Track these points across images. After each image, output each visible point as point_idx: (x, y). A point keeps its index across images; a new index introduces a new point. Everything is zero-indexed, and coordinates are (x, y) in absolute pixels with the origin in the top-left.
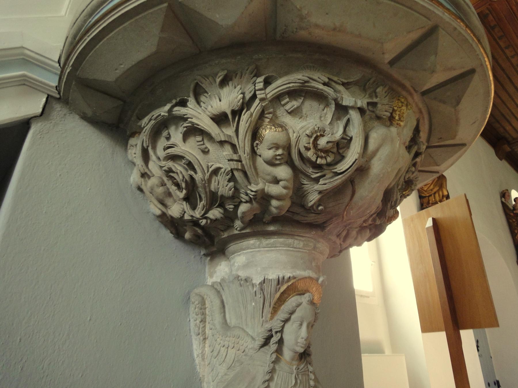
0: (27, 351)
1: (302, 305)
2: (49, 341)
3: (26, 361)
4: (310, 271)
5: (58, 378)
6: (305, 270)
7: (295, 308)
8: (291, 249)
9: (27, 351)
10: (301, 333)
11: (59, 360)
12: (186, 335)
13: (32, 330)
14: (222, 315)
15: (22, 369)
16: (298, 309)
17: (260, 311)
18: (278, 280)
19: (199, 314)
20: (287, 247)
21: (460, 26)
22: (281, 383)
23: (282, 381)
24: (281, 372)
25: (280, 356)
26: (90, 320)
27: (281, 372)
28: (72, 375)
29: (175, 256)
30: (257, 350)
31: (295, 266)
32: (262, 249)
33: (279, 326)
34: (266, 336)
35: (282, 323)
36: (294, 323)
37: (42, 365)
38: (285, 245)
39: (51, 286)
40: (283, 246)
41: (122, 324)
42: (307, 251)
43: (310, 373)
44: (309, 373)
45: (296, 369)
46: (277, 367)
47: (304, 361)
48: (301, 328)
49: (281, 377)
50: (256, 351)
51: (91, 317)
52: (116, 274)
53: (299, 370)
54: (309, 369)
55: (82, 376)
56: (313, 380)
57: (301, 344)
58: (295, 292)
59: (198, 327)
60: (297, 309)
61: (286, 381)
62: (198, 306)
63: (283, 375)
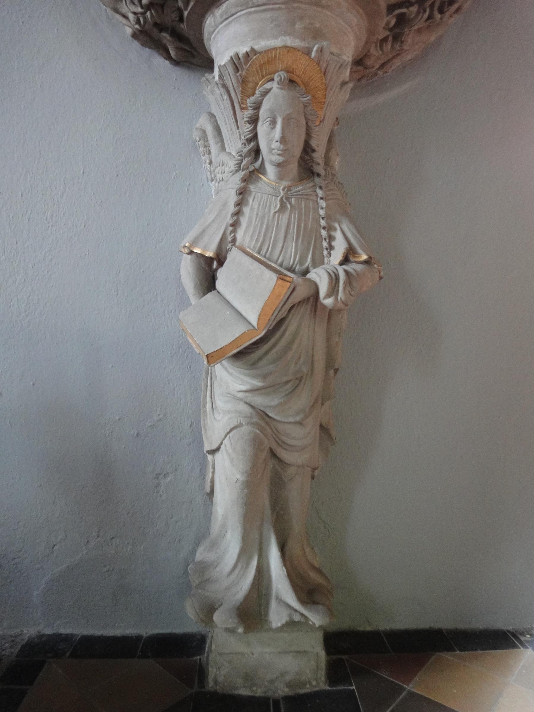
0: (29, 204)
1: (272, 91)
2: (48, 195)
3: (30, 213)
4: (288, 38)
5: (62, 228)
6: (276, 37)
7: (261, 98)
8: (253, 9)
9: (29, 204)
11: (60, 212)
12: (203, 185)
13: (30, 186)
14: (219, 144)
15: (29, 220)
16: (265, 99)
17: (233, 120)
18: (232, 61)
19: (206, 154)
20: (246, 9)
22: (259, 208)
23: (259, 205)
24: (259, 194)
26: (83, 172)
27: (259, 194)
28: (75, 225)
29: (177, 88)
31: (260, 35)
32: (221, 26)
33: (247, 132)
35: (251, 127)
37: (46, 216)
38: (241, 6)
39: (39, 143)
40: (239, 8)
41: (119, 175)
42: (281, 6)
44: (317, 199)
45: (283, 190)
46: (252, 188)
49: (259, 200)
51: (83, 170)
52: (103, 121)
54: (319, 194)
55: (84, 226)
57: (276, 151)
58: (263, 77)
59: (209, 171)
61: (266, 204)
62: (200, 143)
63: (262, 197)
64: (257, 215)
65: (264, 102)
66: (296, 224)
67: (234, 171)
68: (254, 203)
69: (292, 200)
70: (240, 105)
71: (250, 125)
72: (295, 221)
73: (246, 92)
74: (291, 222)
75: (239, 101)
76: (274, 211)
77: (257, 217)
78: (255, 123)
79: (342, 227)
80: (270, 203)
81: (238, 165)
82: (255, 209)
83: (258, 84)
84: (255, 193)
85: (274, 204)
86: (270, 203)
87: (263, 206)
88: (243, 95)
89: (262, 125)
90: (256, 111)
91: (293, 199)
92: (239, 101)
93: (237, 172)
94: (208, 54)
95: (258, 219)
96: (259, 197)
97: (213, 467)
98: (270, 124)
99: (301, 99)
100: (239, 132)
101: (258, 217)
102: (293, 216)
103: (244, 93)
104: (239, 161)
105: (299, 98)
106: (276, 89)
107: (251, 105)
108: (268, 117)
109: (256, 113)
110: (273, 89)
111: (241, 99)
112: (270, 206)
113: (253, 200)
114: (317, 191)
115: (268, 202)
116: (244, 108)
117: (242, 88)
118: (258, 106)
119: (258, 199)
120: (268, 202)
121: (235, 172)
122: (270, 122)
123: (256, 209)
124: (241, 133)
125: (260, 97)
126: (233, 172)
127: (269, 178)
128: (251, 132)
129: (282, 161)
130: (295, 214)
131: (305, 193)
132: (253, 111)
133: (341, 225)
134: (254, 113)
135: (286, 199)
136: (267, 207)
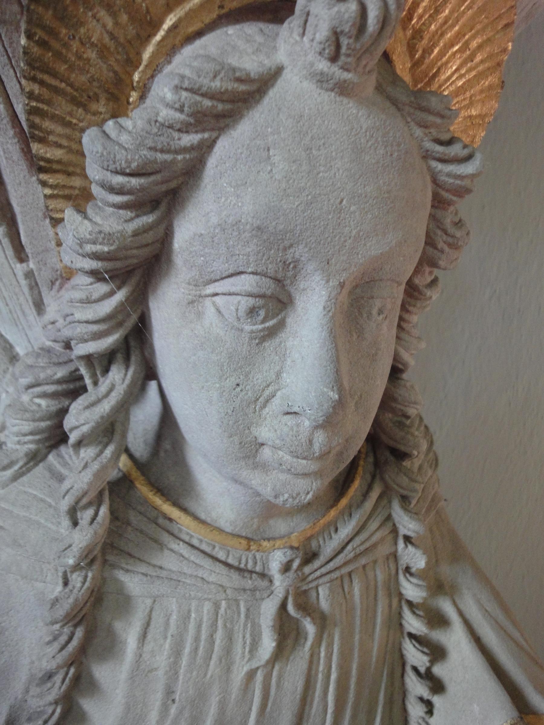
10: (278, 375)
21: (239, 628)
23: (177, 653)
25: (167, 508)
30: (16, 467)
34: (59, 382)
35: (111, 294)
36: (210, 289)
43: (401, 544)
47: (370, 488)
48: (282, 325)
49: (172, 629)
50: (9, 473)
53: (317, 563)
56: (422, 575)
60: (217, 138)
63: (185, 618)
64: (169, 692)
65: (212, 162)
66: (334, 676)
67: (21, 463)
68: (149, 647)
69: (318, 594)
70: (30, 150)
71: (102, 288)
72: (330, 667)
73: (62, 68)
74: (317, 675)
75: (14, 116)
76: (246, 669)
77: (170, 702)
78: (134, 280)
79: (461, 606)
80: (230, 638)
81: (37, 437)
82: (156, 669)
83: (156, 26)
84: (149, 602)
85: (248, 636)
86: (230, 638)
87: (195, 659)
88: (42, 83)
89: (192, 302)
90: (148, 219)
91: (323, 592)
92: (14, 116)
93: (36, 465)
94: (336, 361)
95: (173, 710)
96: (174, 617)
97: (31, 308)
98: (252, 312)
99: (439, 166)
100: (29, 275)
101: (173, 701)
102: (323, 654)
103: (54, 75)
104: (41, 419)
105: (426, 156)
106: (308, 86)
107: (119, 179)
108: (241, 269)
109: (146, 229)
110: (280, 83)
111: (31, 112)
112: (228, 650)
113: (144, 636)
114: (394, 515)
115: (219, 636)
116: (55, 166)
117: (29, 36)
118: (173, 184)
119: (167, 623)
120: (219, 636)
121: (26, 464)
122: (251, 301)
123: (161, 673)
124: (43, 276)
125: (185, 129)
126: (16, 467)
127: (214, 514)
128: (113, 323)
129: (310, 496)
130: (330, 646)
131: (362, 548)
132: (129, 214)
133: (458, 601)
134: (136, 234)
135: (299, 607)
136: (215, 657)
